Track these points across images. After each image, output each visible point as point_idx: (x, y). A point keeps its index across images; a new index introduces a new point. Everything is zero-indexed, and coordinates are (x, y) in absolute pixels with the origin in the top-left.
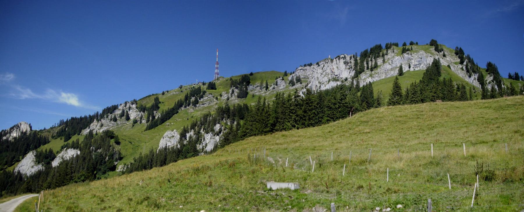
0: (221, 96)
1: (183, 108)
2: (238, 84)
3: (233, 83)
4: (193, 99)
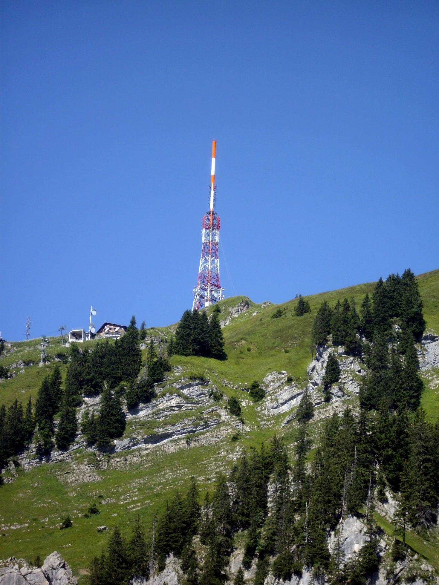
0: (257, 393)
1: (27, 461)
2: (363, 331)
3: (337, 325)
4: (91, 405)
